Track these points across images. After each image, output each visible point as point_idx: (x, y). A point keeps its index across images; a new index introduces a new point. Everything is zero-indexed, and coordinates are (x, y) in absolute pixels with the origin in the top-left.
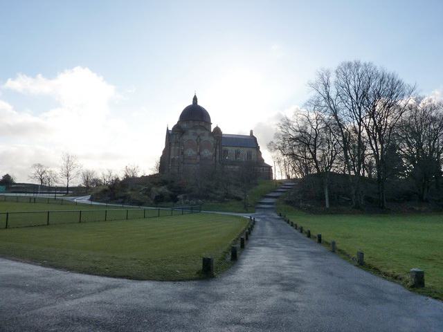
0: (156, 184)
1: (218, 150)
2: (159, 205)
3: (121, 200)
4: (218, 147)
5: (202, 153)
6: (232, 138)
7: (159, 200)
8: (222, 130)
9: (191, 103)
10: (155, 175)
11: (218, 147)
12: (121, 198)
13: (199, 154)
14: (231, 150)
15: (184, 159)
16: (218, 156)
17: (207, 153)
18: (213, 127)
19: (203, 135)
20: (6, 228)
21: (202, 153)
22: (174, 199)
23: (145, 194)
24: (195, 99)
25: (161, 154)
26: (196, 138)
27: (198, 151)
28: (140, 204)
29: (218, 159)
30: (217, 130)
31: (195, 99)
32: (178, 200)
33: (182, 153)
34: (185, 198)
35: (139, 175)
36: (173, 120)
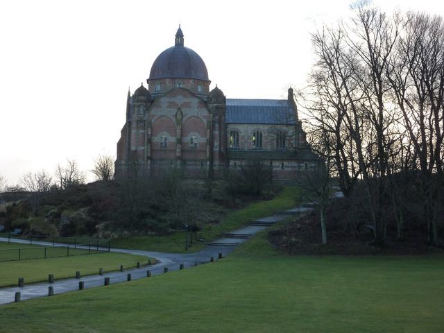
0: (273, 195)
1: (217, 133)
2: (69, 239)
3: (18, 231)
4: (217, 126)
5: (187, 139)
6: (256, 108)
7: (70, 232)
8: (225, 93)
9: (171, 43)
10: (97, 182)
11: (217, 126)
12: (19, 227)
13: (180, 141)
14: (246, 131)
15: (182, 151)
16: (216, 144)
17: (197, 138)
18: (211, 88)
19: (187, 105)
20: (68, 256)
21: (187, 139)
22: (90, 229)
23: (52, 222)
24: (179, 35)
25: (118, 136)
26: (174, 111)
27: (178, 137)
28: (42, 237)
29: (216, 149)
30: (217, 92)
31: (179, 35)
32: (95, 231)
33: (150, 141)
34: (106, 228)
35: (86, 183)
36: (140, 77)
